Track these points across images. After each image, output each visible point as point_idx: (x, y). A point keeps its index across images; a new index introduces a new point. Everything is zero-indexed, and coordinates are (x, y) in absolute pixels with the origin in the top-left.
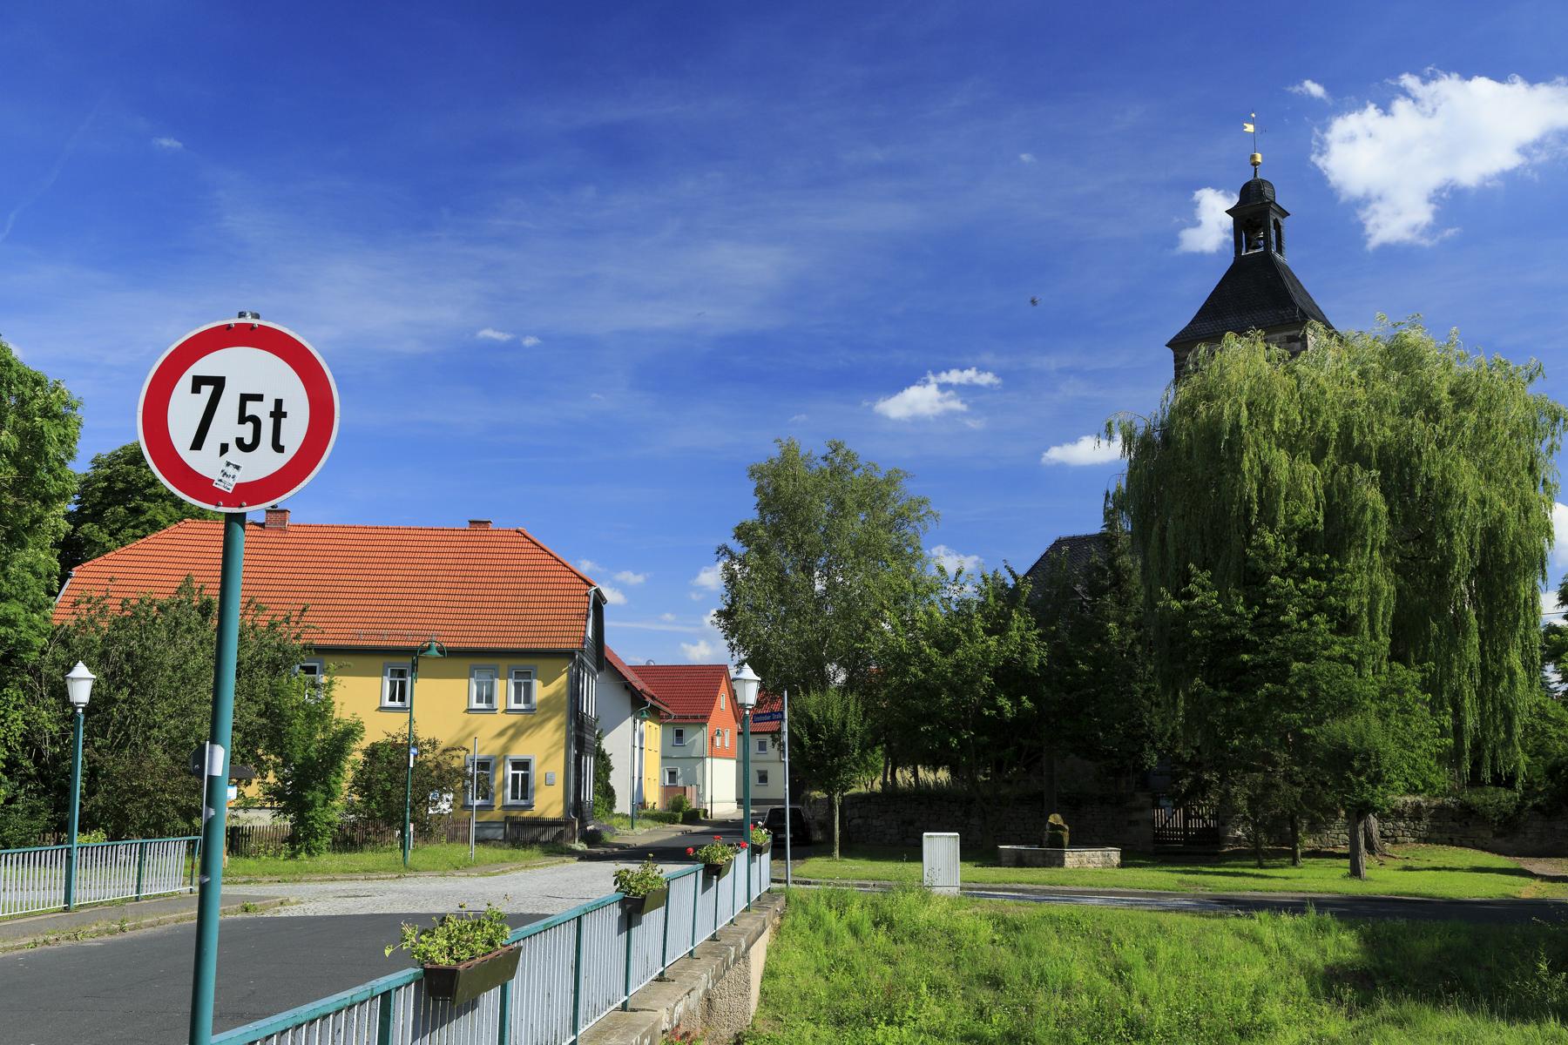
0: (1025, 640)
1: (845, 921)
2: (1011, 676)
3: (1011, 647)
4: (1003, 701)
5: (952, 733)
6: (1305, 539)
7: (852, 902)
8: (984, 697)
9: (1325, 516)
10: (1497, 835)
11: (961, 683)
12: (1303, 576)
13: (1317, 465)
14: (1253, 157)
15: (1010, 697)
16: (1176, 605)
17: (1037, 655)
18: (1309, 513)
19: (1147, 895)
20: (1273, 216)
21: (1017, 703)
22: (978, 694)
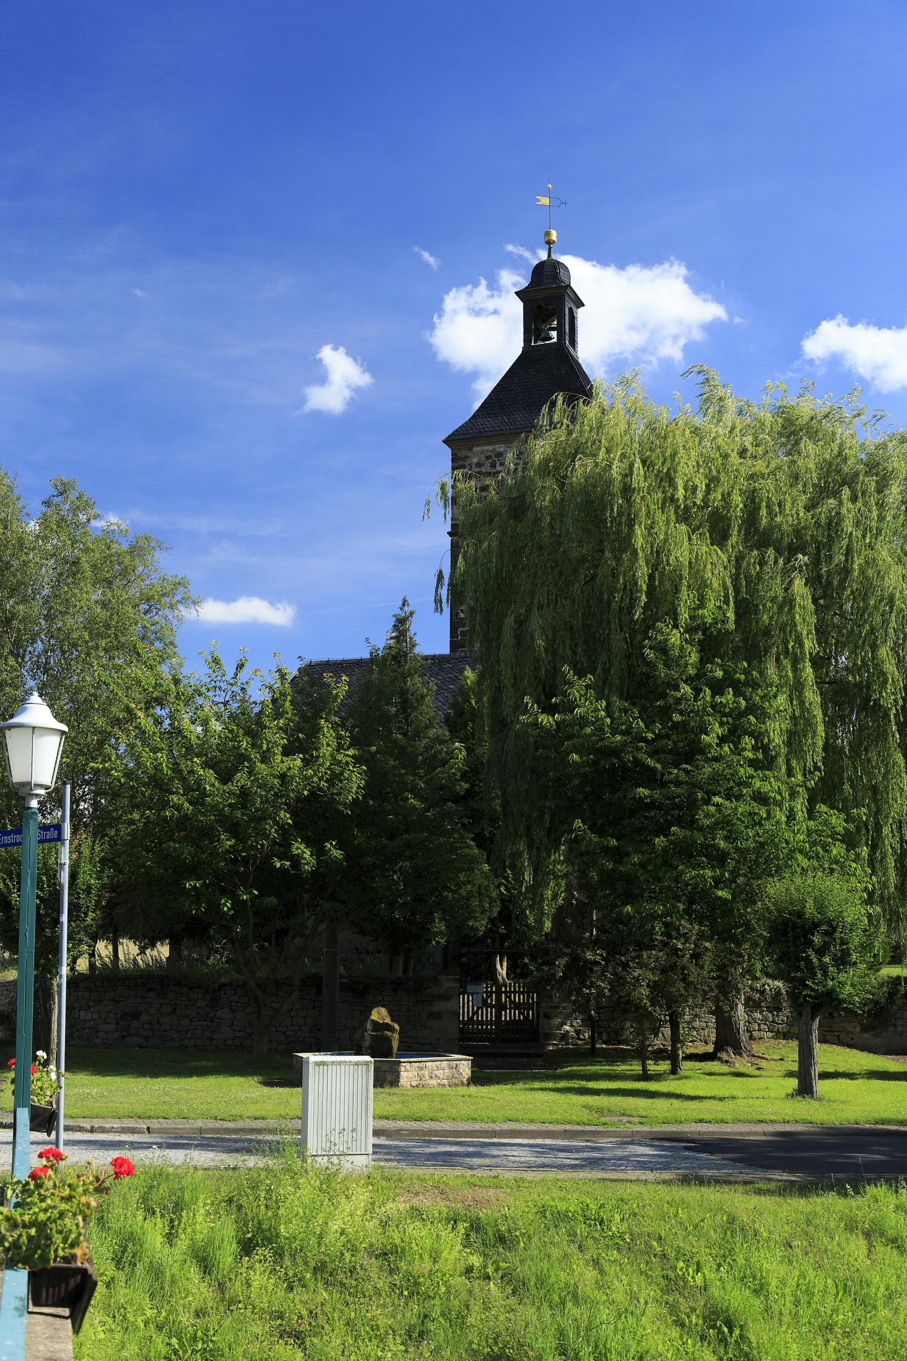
0: (338, 764)
1: (183, 1243)
2: (315, 814)
3: (318, 776)
4: (299, 847)
5: (223, 892)
6: (710, 643)
7: (194, 1200)
8: (274, 843)
9: (736, 613)
10: (865, 1029)
11: (243, 817)
12: (718, 688)
13: (722, 546)
14: (548, 234)
15: (308, 843)
16: (545, 719)
17: (355, 782)
18: (719, 611)
19: (566, 1134)
20: (568, 304)
21: (319, 852)
22: (267, 836)
